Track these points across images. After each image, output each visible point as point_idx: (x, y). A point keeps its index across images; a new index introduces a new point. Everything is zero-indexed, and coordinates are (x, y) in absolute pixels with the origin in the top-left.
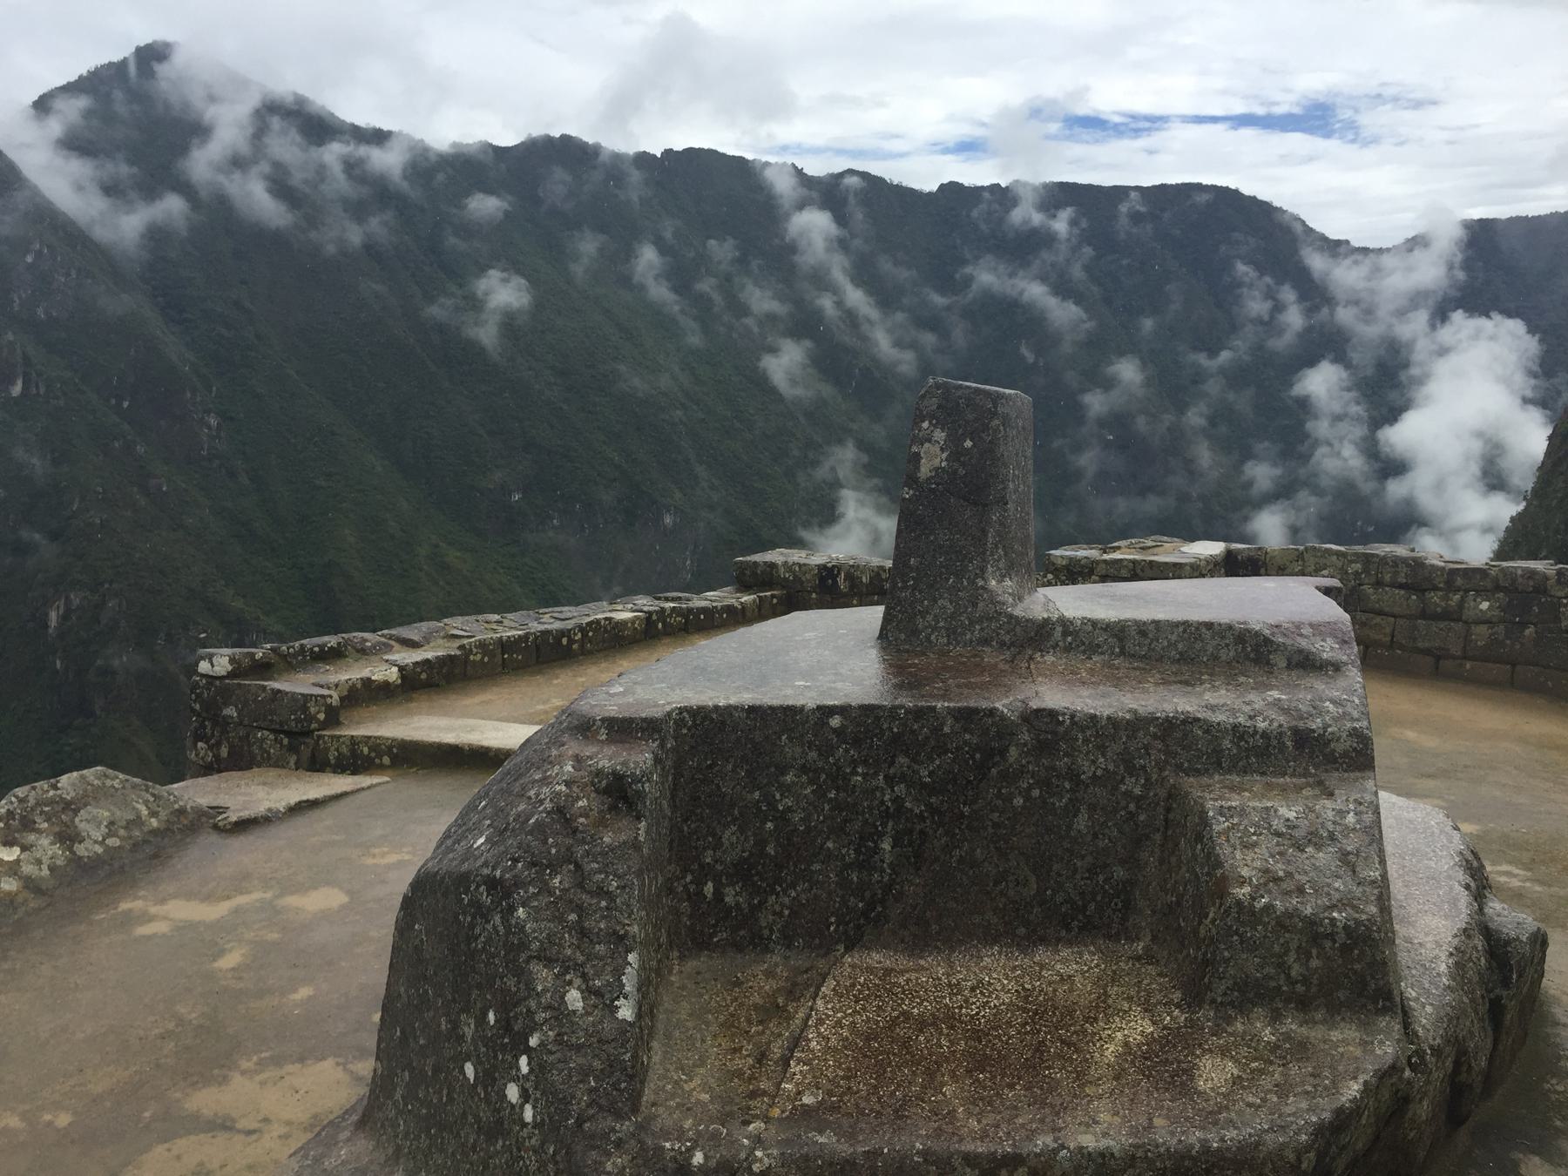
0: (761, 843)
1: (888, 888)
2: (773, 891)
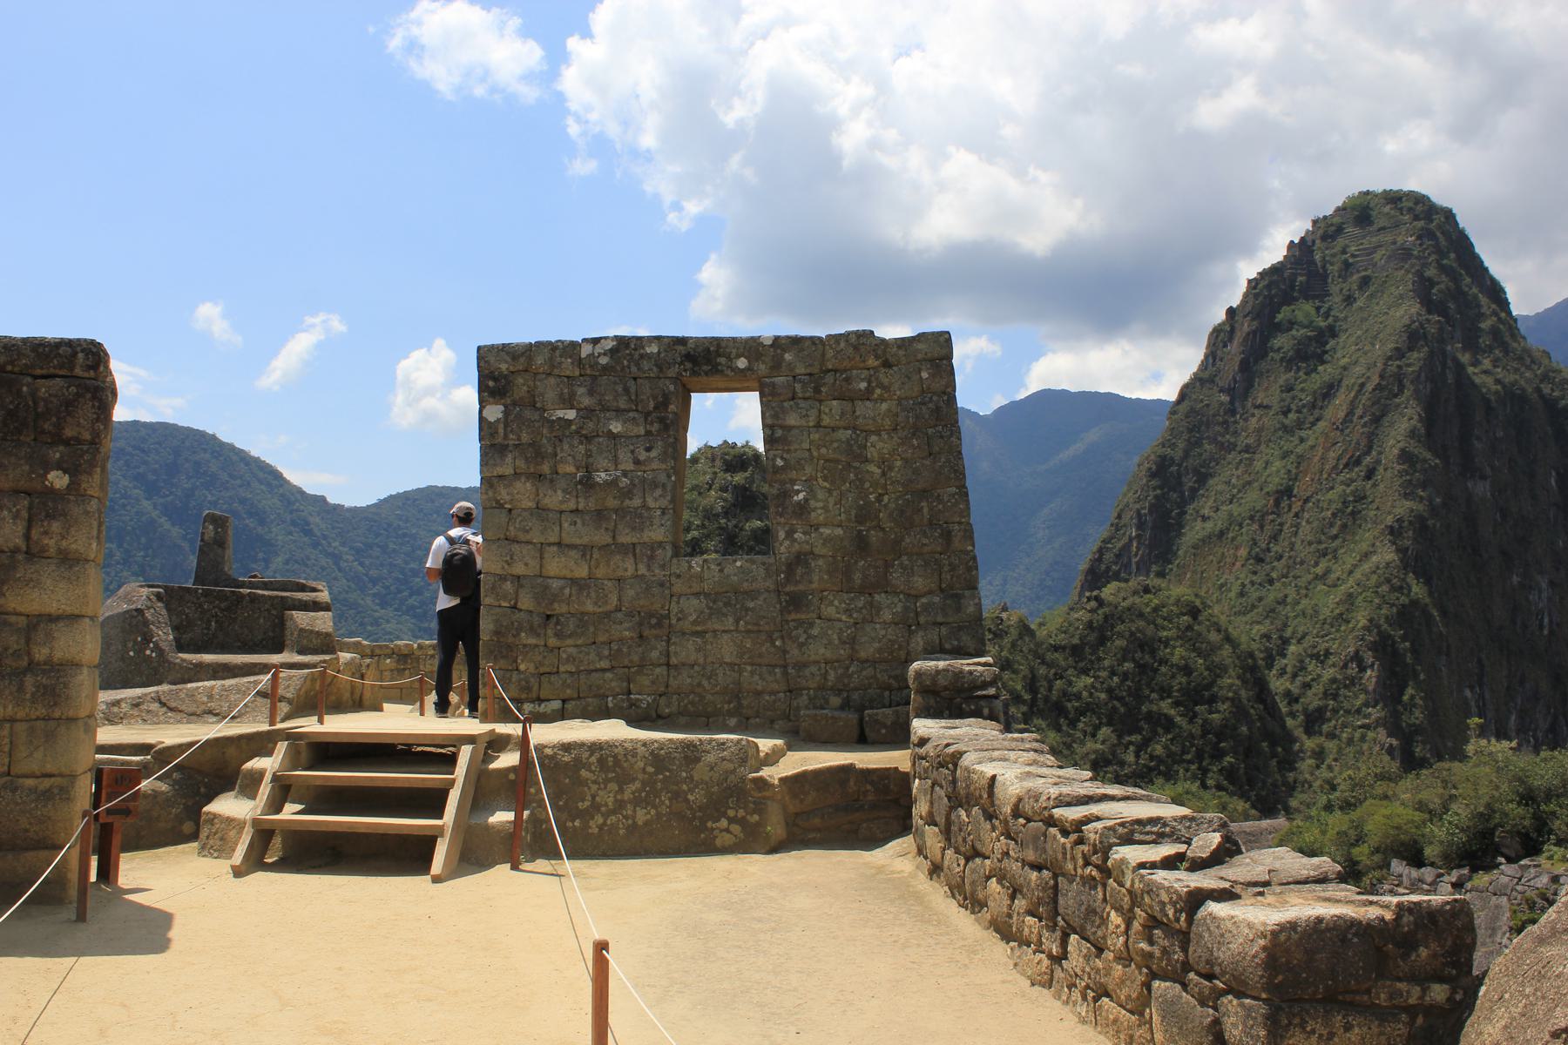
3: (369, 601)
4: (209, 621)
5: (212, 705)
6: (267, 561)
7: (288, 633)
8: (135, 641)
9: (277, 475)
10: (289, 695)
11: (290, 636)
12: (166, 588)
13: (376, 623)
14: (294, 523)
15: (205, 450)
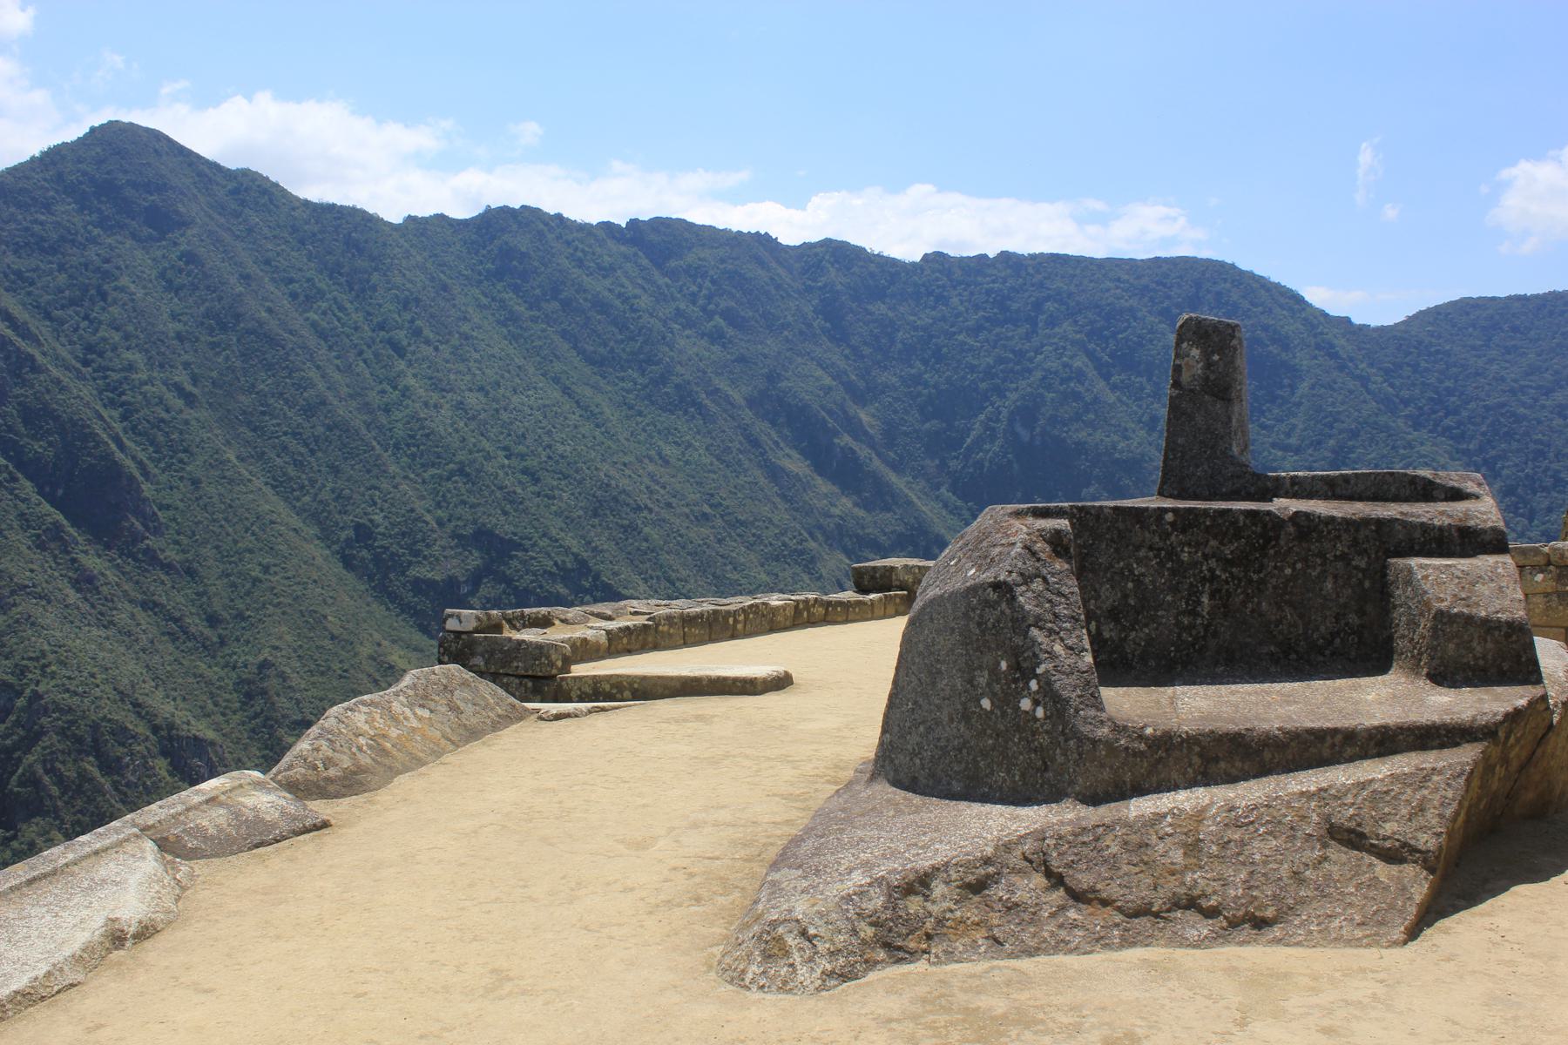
0: (1125, 596)
1: (1206, 628)
2: (1133, 629)
3: (1400, 422)
4: (1194, 594)
5: (1197, 879)
6: (1293, 388)
7: (1400, 616)
8: (994, 671)
9: (1298, 300)
10: (1426, 841)
11: (1410, 632)
12: (1081, 517)
13: (1410, 446)
14: (1318, 347)
15: (1225, 280)
